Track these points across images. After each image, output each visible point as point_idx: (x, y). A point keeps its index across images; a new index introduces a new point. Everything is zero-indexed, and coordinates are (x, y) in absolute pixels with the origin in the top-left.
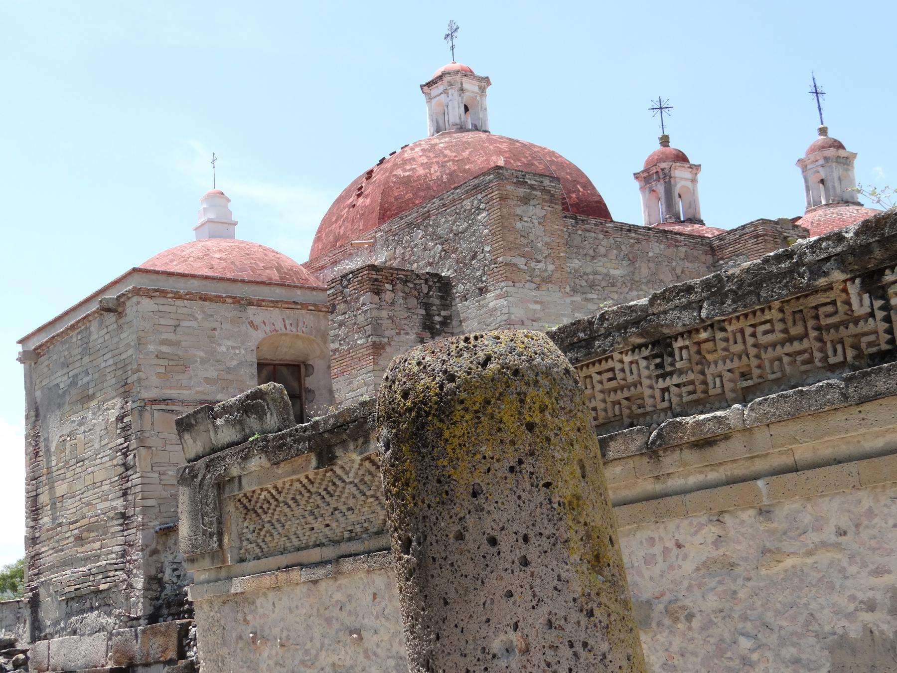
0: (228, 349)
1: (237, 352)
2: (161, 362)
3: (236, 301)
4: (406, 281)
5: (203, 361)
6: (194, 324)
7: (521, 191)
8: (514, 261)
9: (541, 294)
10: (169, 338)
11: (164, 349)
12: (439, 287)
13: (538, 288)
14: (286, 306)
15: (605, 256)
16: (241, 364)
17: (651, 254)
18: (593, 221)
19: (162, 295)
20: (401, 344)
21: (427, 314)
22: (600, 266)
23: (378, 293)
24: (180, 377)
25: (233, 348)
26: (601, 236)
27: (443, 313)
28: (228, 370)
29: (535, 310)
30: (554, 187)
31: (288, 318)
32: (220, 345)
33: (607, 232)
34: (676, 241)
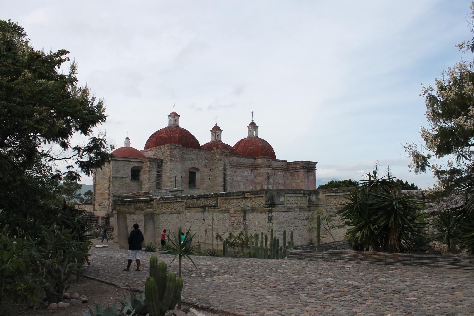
22: (191, 156)
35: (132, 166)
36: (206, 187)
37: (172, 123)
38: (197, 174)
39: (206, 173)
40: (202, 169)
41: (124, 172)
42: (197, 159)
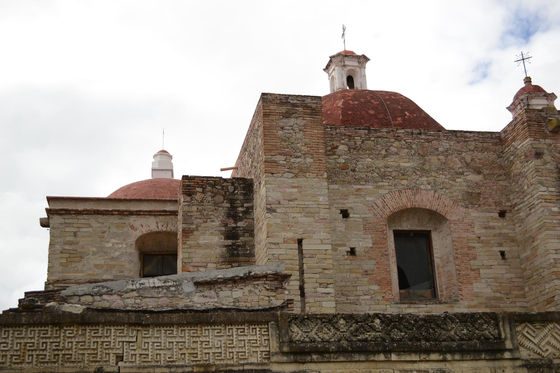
0: (113, 245)
1: (120, 246)
2: (64, 255)
3: (121, 213)
4: (215, 185)
5: (94, 254)
6: (90, 230)
7: (284, 109)
8: (274, 158)
9: (301, 181)
10: (71, 239)
11: (67, 247)
12: (243, 187)
13: (296, 176)
14: (159, 213)
15: (397, 154)
16: (122, 254)
17: (441, 149)
18: (385, 130)
19: (67, 212)
20: (207, 229)
21: (232, 207)
22: (391, 161)
23: (189, 195)
24: (77, 264)
25: (117, 244)
26: (393, 140)
27: (245, 205)
28: (112, 259)
29: (291, 193)
30: (316, 103)
31: (161, 221)
32: (108, 242)
33: (398, 136)
34: (466, 137)
35: (138, 234)
36: (488, 292)
37: (341, 83)
38: (435, 236)
39: (478, 231)
40: (455, 214)
41: (100, 261)
42: (424, 172)
